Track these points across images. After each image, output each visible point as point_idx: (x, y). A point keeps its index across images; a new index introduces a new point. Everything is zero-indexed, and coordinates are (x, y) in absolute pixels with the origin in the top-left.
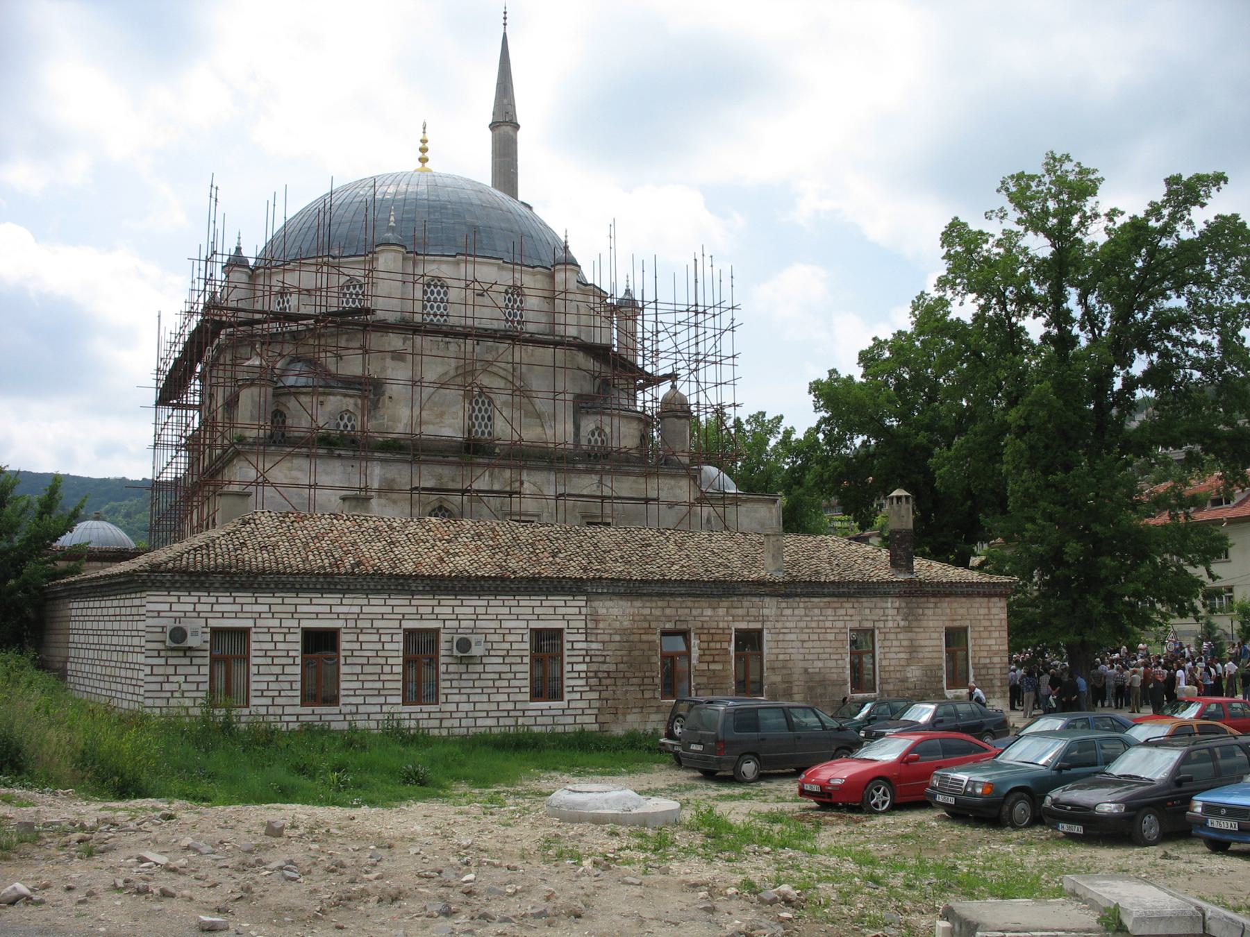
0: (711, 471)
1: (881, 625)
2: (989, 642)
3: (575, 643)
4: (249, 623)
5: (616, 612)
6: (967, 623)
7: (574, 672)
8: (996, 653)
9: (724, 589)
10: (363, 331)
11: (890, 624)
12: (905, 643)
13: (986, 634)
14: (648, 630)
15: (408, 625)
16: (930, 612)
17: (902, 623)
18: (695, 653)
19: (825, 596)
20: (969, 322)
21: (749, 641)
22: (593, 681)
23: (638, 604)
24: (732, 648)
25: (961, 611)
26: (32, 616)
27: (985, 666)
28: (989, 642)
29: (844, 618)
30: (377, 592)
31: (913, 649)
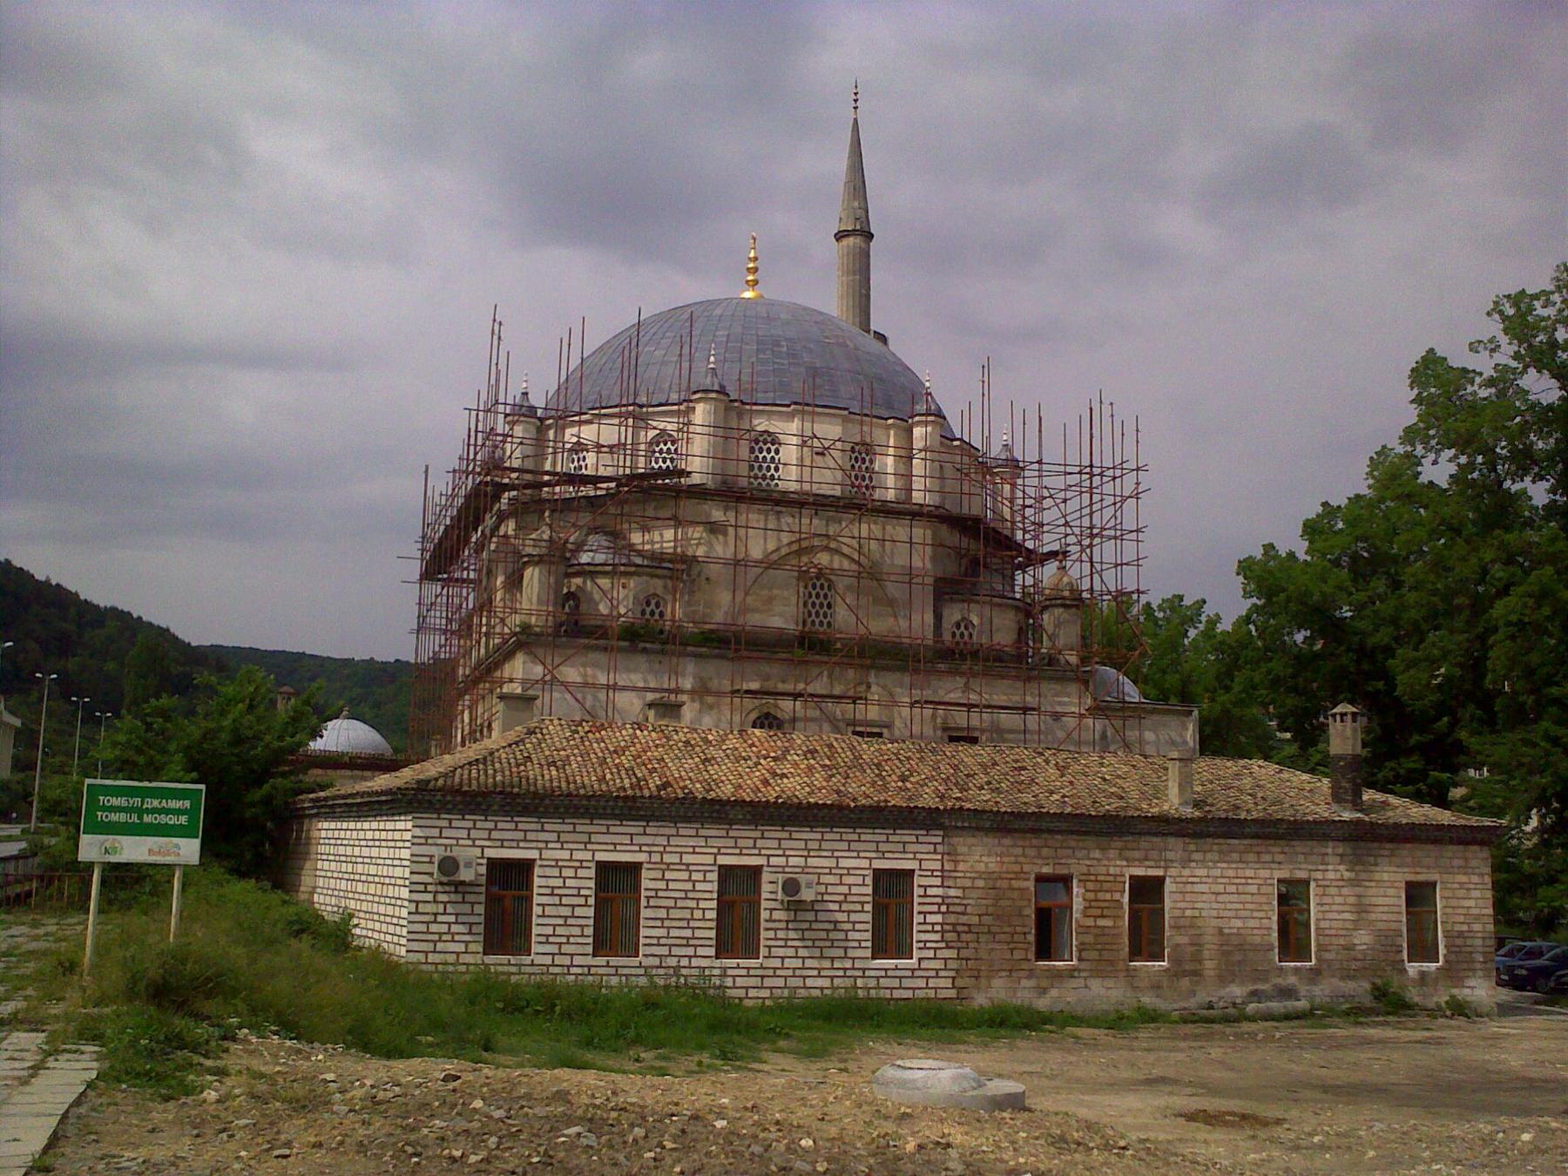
1: (1319, 875)
8: (1478, 917)
11: (1331, 875)
12: (1352, 900)
13: (1462, 893)
17: (1347, 875)
21: (1147, 891)
22: (950, 936)
24: (1126, 899)
27: (1461, 934)
31: (1361, 909)
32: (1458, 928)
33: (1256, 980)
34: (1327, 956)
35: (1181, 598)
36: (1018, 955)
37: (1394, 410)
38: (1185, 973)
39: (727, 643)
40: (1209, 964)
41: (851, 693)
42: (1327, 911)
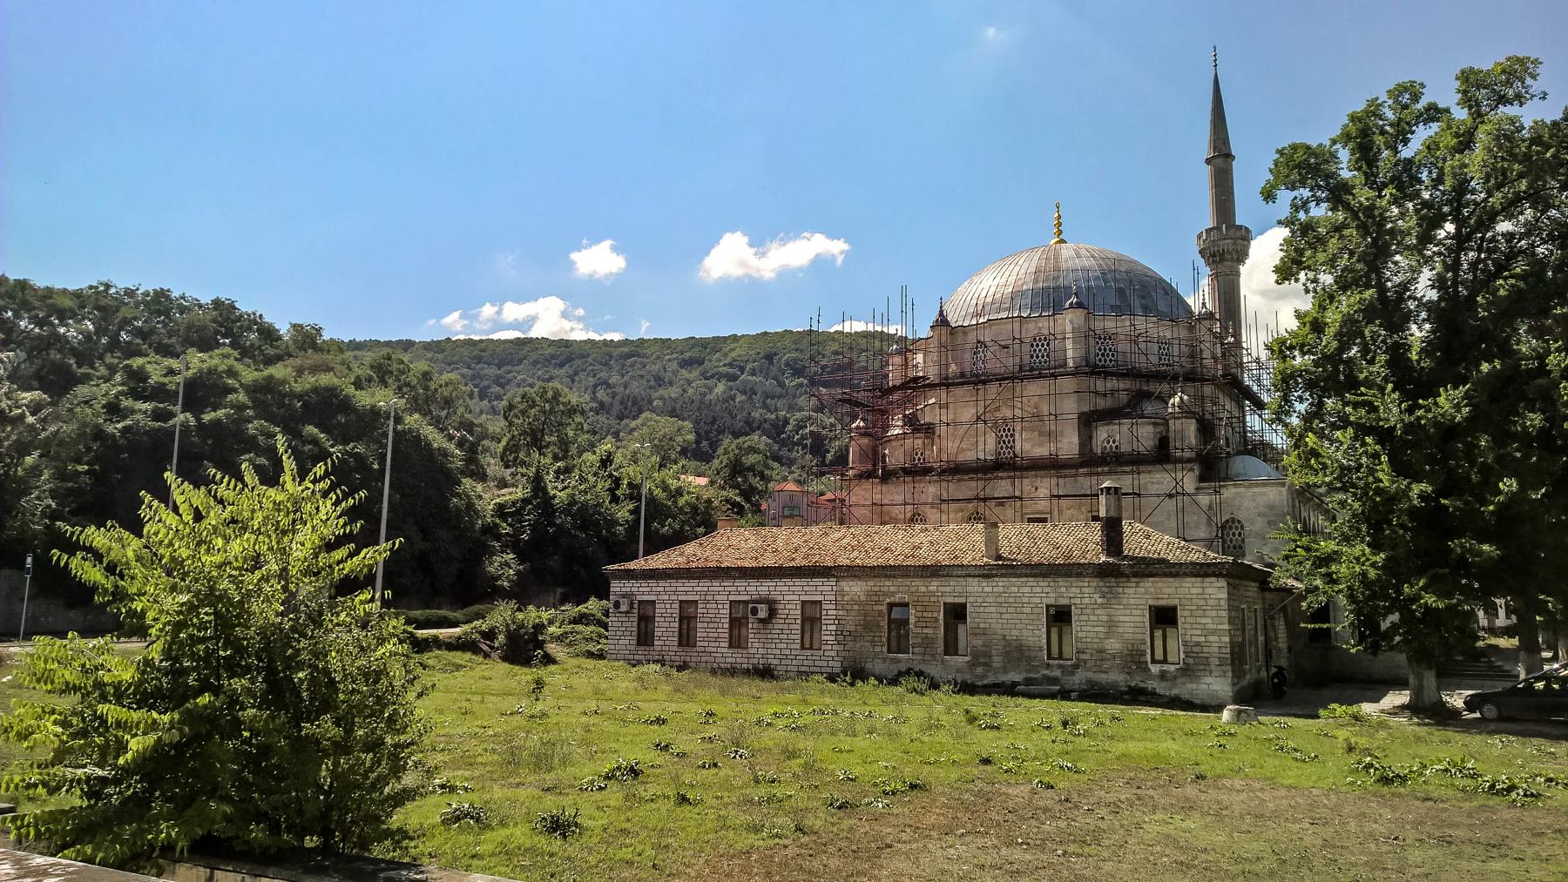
0: (311, 429)
1: (1078, 601)
2: (1204, 621)
3: (830, 611)
4: (653, 598)
5: (855, 589)
6: (1176, 602)
7: (828, 629)
8: (1214, 632)
9: (933, 571)
10: (947, 378)
11: (1087, 601)
12: (1105, 618)
13: (1200, 613)
14: (878, 603)
15: (732, 598)
16: (1132, 591)
17: (1100, 601)
18: (912, 620)
19: (1020, 576)
20: (574, 256)
21: (957, 613)
22: (840, 638)
23: (871, 583)
24: (941, 617)
25: (1167, 590)
26: (36, 454)
27: (1198, 644)
28: (1204, 621)
29: (1042, 594)
30: (716, 578)
31: (1111, 625)
32: (1196, 639)
33: (1029, 671)
34: (1083, 656)
35: (108, 286)
36: (878, 649)
37: (1346, 121)
38: (980, 664)
39: (956, 470)
40: (996, 659)
41: (982, 495)
42: (1085, 629)
